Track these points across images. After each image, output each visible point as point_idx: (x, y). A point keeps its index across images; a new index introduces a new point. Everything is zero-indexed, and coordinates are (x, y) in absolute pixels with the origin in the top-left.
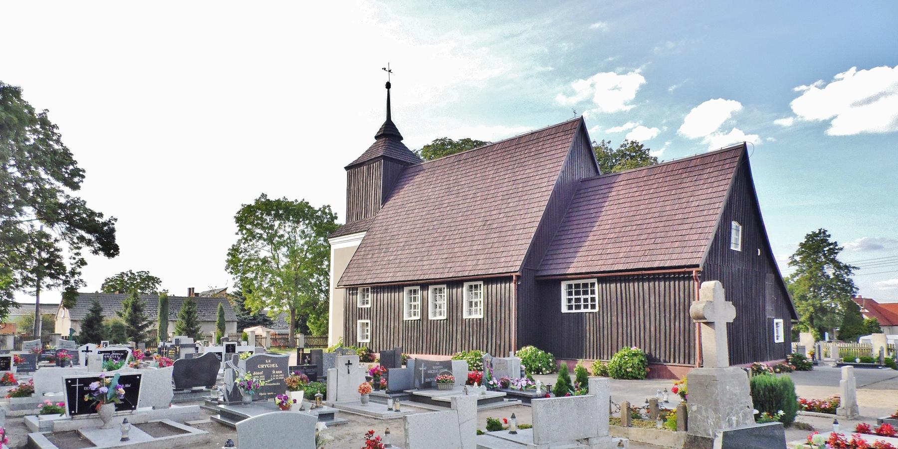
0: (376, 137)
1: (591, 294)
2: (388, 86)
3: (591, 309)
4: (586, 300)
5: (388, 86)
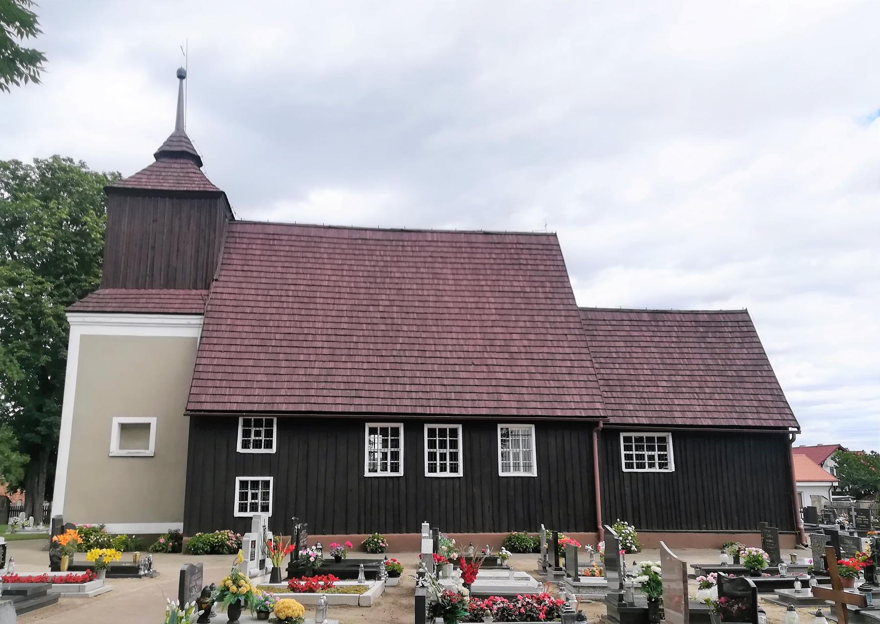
0: (157, 156)
1: (451, 448)
2: (181, 75)
3: (392, 471)
4: (651, 458)
5: (181, 75)
